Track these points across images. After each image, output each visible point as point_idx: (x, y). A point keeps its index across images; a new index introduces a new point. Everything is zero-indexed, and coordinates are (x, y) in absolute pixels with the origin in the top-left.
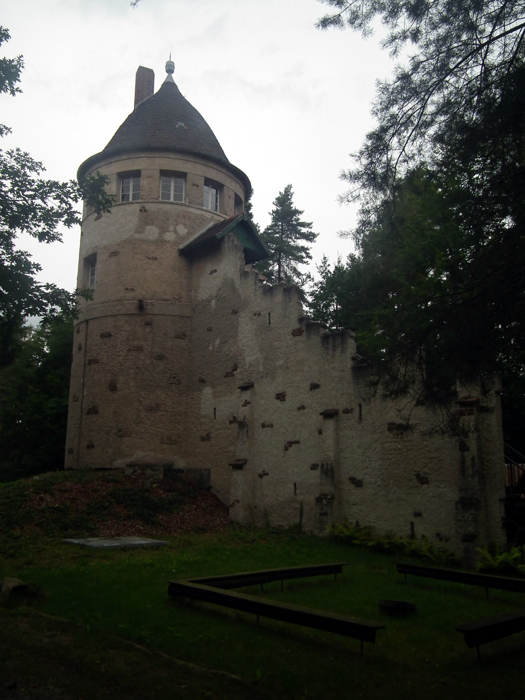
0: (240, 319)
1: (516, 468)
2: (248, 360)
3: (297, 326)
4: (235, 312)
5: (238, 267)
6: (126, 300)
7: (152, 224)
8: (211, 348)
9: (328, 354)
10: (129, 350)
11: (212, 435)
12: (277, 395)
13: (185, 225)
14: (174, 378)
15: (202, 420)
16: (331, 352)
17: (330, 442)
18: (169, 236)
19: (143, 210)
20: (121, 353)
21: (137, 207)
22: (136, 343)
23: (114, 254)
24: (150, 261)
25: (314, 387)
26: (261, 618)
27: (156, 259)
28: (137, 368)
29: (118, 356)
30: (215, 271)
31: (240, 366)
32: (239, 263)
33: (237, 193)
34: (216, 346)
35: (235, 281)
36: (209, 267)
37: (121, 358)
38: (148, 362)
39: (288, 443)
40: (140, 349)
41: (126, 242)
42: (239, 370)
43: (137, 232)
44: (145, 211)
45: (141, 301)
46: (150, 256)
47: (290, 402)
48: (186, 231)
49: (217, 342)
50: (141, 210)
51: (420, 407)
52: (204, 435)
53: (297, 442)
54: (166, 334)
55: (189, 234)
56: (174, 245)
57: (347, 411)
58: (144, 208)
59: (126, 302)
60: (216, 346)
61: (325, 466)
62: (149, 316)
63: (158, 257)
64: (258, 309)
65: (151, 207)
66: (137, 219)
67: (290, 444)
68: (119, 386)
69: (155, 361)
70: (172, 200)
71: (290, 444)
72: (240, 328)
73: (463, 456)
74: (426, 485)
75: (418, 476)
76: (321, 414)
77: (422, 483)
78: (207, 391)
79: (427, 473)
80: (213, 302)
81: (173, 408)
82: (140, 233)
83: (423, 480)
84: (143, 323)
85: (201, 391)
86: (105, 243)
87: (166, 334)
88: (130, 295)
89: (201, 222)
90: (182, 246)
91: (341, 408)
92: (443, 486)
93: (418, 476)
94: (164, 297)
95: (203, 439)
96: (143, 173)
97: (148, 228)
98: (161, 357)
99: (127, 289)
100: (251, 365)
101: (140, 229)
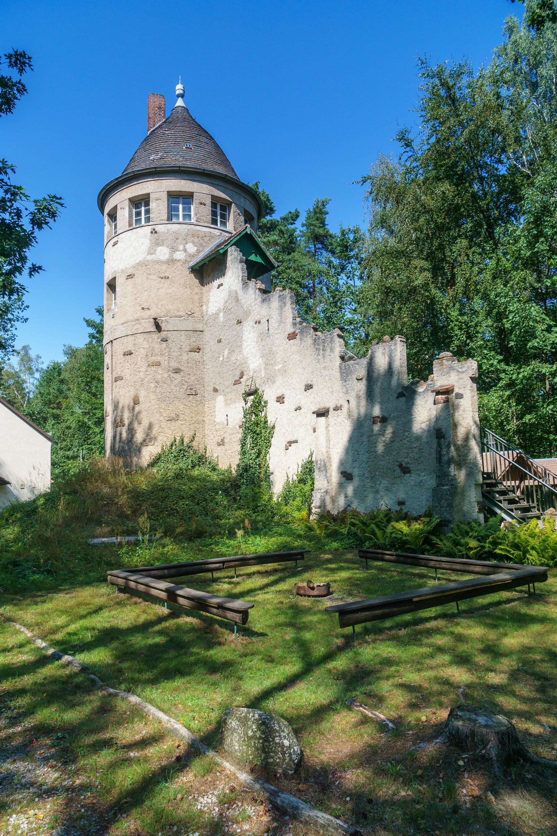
1: (498, 456)
3: (291, 330)
4: (239, 322)
5: (240, 278)
6: (143, 319)
7: (163, 245)
8: (221, 359)
10: (149, 365)
11: (226, 441)
12: (277, 398)
13: (193, 242)
14: (191, 389)
17: (323, 439)
19: (154, 232)
20: (142, 369)
21: (148, 229)
23: (130, 276)
24: (163, 280)
25: (309, 387)
27: (168, 278)
28: (156, 382)
29: (139, 372)
30: (222, 285)
31: (245, 373)
32: (241, 274)
33: (247, 209)
34: (226, 356)
35: (239, 292)
37: (142, 374)
39: (288, 442)
40: (158, 364)
41: (141, 264)
43: (150, 253)
44: (156, 232)
45: (155, 319)
46: (162, 276)
47: (290, 403)
48: (196, 248)
49: (226, 352)
50: (152, 232)
51: (401, 399)
52: (220, 441)
53: (296, 442)
54: (181, 348)
55: (198, 251)
56: (185, 263)
57: (336, 409)
58: (154, 230)
59: (142, 321)
60: (226, 356)
61: (319, 462)
62: (164, 333)
63: (170, 276)
64: (259, 316)
66: (149, 241)
67: (290, 443)
69: (172, 375)
70: (181, 220)
71: (290, 443)
72: (244, 337)
74: (408, 475)
75: (400, 466)
77: (405, 473)
78: (220, 399)
79: (408, 463)
80: (221, 314)
81: (192, 418)
82: (152, 254)
83: (405, 470)
84: (159, 340)
85: (215, 400)
87: (181, 348)
88: (147, 313)
89: (210, 240)
90: (192, 264)
91: (331, 406)
92: (423, 474)
93: (400, 466)
94: (178, 314)
95: (219, 445)
96: (152, 197)
97: (159, 249)
98: (177, 371)
99: (143, 309)
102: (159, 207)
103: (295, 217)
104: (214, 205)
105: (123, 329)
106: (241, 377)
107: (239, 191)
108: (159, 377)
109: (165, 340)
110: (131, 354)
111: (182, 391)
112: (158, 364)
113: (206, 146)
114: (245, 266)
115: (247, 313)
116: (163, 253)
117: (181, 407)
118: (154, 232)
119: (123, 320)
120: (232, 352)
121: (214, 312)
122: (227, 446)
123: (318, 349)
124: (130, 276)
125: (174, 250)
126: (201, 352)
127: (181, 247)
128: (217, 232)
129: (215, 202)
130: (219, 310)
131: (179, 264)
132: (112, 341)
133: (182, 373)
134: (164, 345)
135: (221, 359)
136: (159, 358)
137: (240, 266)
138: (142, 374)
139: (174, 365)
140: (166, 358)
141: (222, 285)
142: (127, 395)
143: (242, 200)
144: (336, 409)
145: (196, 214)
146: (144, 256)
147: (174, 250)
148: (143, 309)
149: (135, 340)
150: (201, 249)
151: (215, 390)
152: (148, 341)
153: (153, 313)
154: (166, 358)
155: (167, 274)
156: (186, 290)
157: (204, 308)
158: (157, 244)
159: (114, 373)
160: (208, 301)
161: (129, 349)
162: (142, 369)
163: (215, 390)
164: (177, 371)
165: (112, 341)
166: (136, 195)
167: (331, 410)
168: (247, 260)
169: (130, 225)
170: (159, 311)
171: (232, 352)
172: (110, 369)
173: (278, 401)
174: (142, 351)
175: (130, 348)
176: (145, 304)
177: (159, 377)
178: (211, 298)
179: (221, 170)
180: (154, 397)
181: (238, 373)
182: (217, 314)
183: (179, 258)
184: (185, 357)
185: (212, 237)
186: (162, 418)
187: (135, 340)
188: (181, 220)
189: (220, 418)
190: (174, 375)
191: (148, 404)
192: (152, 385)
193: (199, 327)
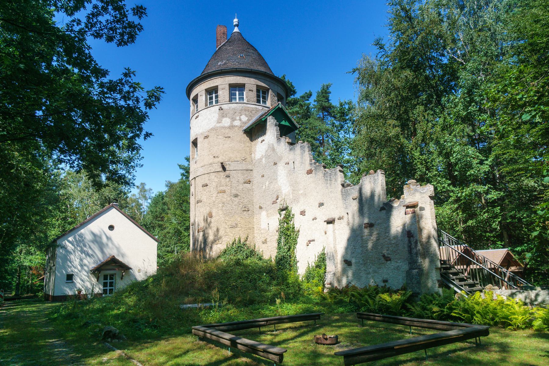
0: (278, 168)
1: (450, 249)
2: (284, 192)
7: (226, 117)
8: (264, 187)
9: (327, 184)
10: (218, 193)
11: (268, 240)
13: (246, 115)
15: (262, 231)
16: (329, 182)
17: (331, 238)
18: (237, 123)
19: (221, 109)
21: (217, 108)
22: (221, 188)
23: (206, 137)
25: (321, 205)
26: (481, 338)
30: (264, 140)
36: (260, 139)
37: (214, 198)
38: (229, 199)
40: (224, 192)
42: (279, 199)
44: (222, 109)
45: (222, 163)
49: (267, 183)
53: (314, 241)
55: (249, 120)
57: (340, 219)
65: (223, 107)
67: (310, 241)
68: (214, 214)
70: (237, 101)
71: (310, 241)
73: (410, 242)
74: (389, 262)
76: (325, 221)
77: (387, 261)
78: (264, 213)
82: (220, 123)
83: (387, 259)
86: (201, 131)
88: (216, 160)
90: (245, 128)
94: (236, 160)
95: (263, 243)
97: (224, 119)
98: (236, 196)
99: (214, 157)
100: (286, 195)
101: (219, 121)
102: (224, 94)
103: (310, 95)
104: (258, 91)
113: (253, 55)
118: (221, 109)
128: (260, 108)
129: (259, 89)
145: (247, 97)
150: (250, 118)
168: (279, 124)
179: (262, 69)
188: (237, 101)
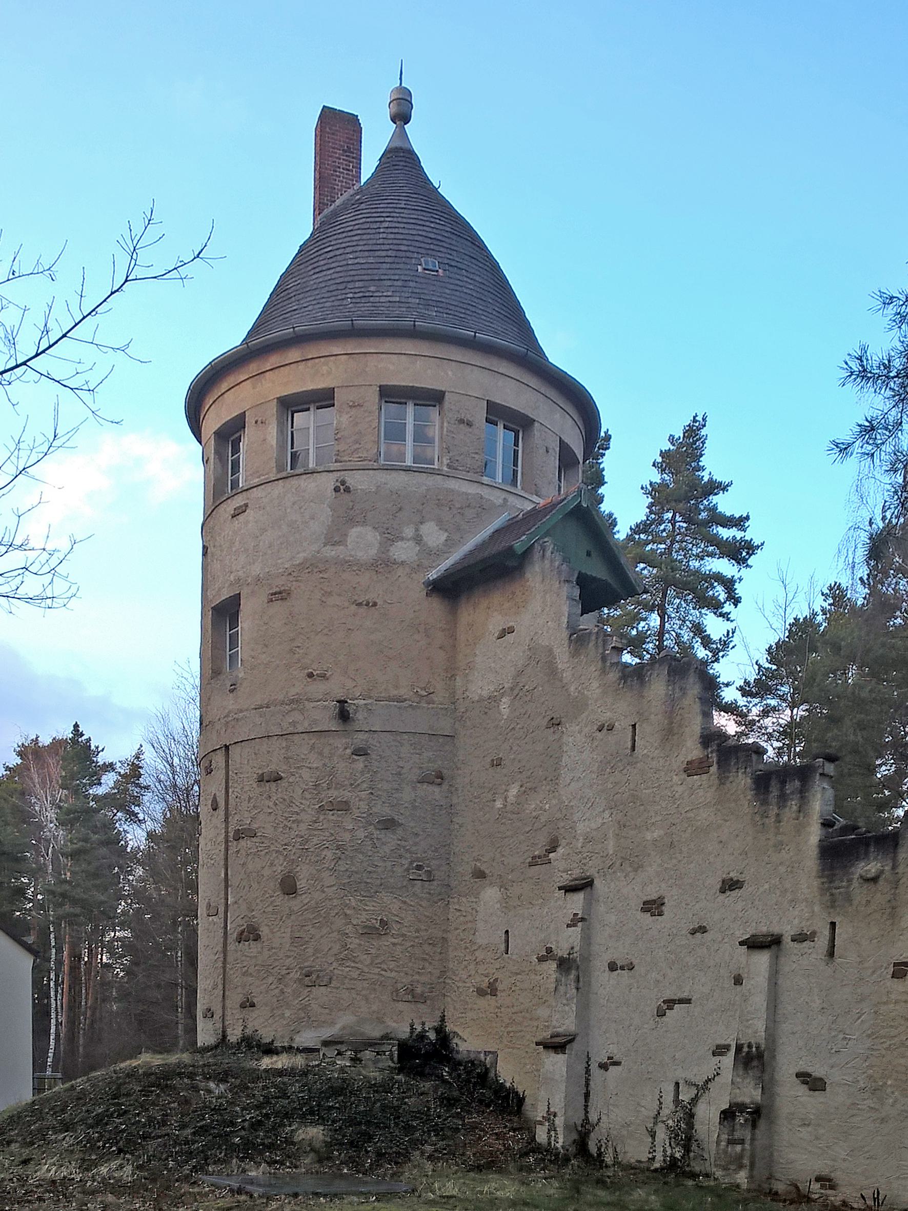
4: (555, 723)
6: (308, 700)
7: (364, 523)
8: (499, 804)
11: (500, 987)
13: (440, 522)
14: (419, 868)
20: (303, 816)
23: (280, 596)
24: (363, 610)
25: (730, 885)
27: (375, 604)
30: (511, 630)
31: (563, 842)
34: (511, 799)
35: (557, 651)
37: (303, 827)
40: (344, 807)
41: (311, 566)
43: (331, 541)
44: (347, 490)
49: (514, 791)
50: (337, 490)
52: (485, 985)
53: (688, 1001)
54: (400, 774)
55: (450, 544)
57: (800, 938)
58: (343, 483)
60: (511, 799)
62: (361, 736)
63: (379, 602)
67: (671, 1003)
69: (376, 833)
71: (671, 1003)
78: (491, 894)
81: (417, 931)
84: (348, 751)
95: (481, 992)
97: (354, 532)
98: (389, 824)
99: (310, 675)
105: (258, 720)
106: (553, 849)
107: (552, 393)
108: (347, 836)
109: (360, 752)
110: (278, 779)
111: (399, 870)
112: (344, 807)
114: (577, 592)
115: (579, 705)
116: (363, 541)
117: (395, 906)
119: (258, 700)
120: (527, 791)
121: (485, 693)
122: (502, 998)
123: (765, 802)
124: (280, 596)
125: (390, 537)
126: (445, 786)
127: (409, 532)
130: (501, 692)
131: (400, 572)
132: (227, 747)
133: (400, 831)
134: (360, 763)
135: (499, 804)
136: (346, 795)
137: (565, 589)
138: (303, 827)
139: (382, 810)
140: (363, 795)
141: (511, 630)
142: (267, 872)
143: (557, 416)
144: (800, 938)
146: (315, 547)
147: (390, 537)
148: (310, 675)
149: (287, 748)
151: (480, 875)
152: (321, 754)
153: (336, 687)
154: (363, 795)
155: (370, 597)
156: (416, 637)
157: (459, 681)
158: (351, 521)
159: (233, 821)
160: (470, 667)
161: (273, 767)
162: (303, 816)
163: (480, 875)
164: (389, 824)
165: (227, 747)
166: (290, 393)
167: (787, 939)
169: (280, 468)
170: (350, 684)
171: (527, 791)
172: (221, 811)
173: (644, 910)
174: (306, 774)
175: (275, 765)
176: (315, 666)
177: (347, 836)
178: (478, 659)
180: (332, 880)
181: (542, 840)
182: (493, 699)
183: (403, 557)
184: (407, 795)
185: (483, 509)
186: (349, 929)
187: (287, 748)
189: (488, 934)
190: (382, 835)
191: (318, 896)
192: (329, 854)
193: (445, 725)
